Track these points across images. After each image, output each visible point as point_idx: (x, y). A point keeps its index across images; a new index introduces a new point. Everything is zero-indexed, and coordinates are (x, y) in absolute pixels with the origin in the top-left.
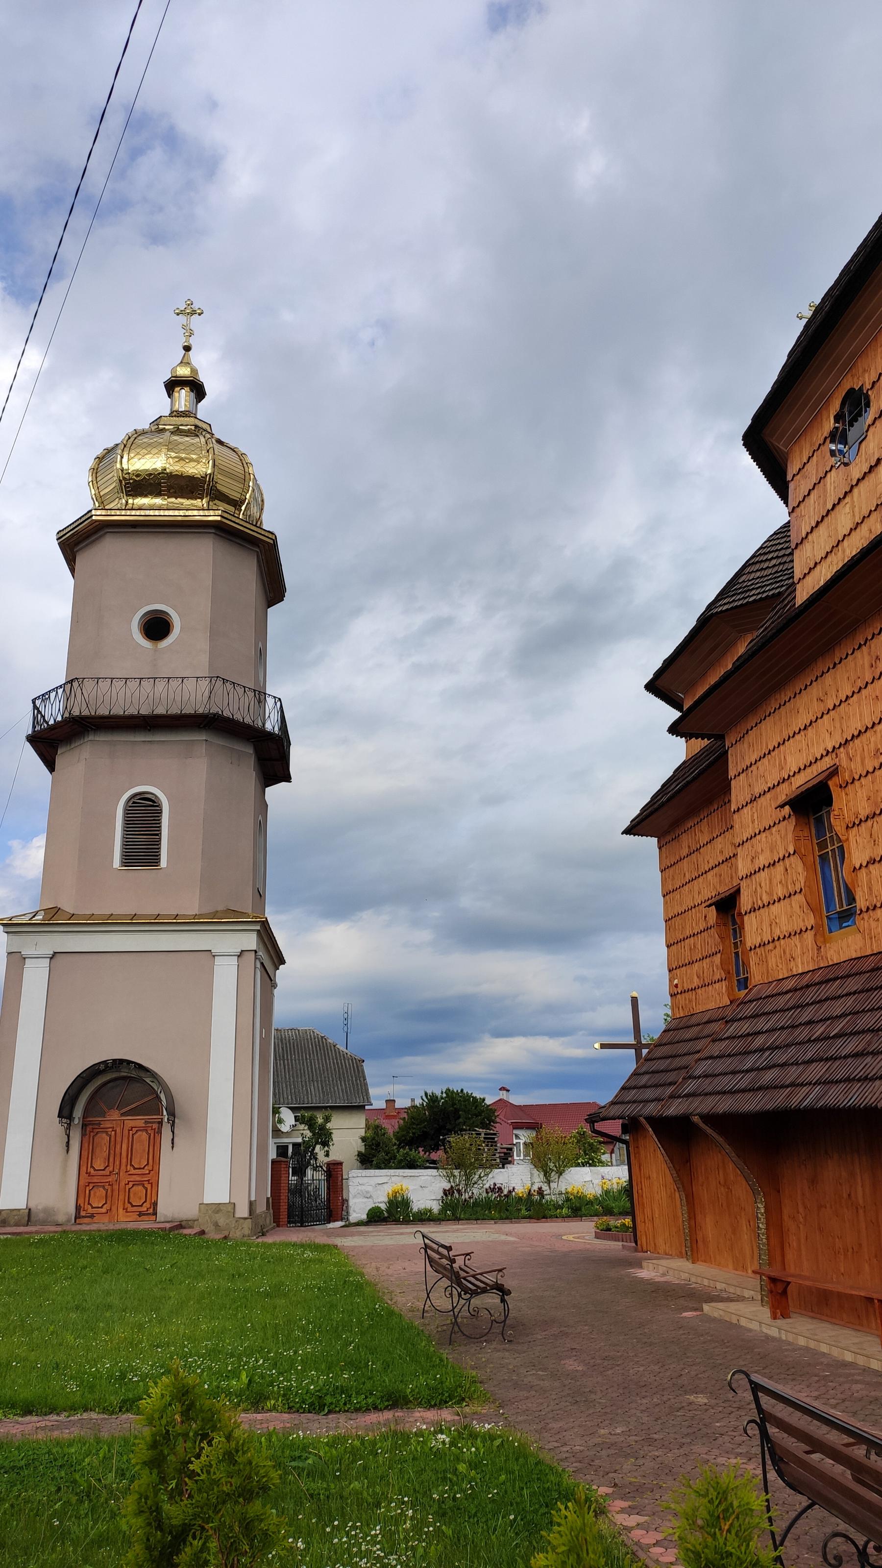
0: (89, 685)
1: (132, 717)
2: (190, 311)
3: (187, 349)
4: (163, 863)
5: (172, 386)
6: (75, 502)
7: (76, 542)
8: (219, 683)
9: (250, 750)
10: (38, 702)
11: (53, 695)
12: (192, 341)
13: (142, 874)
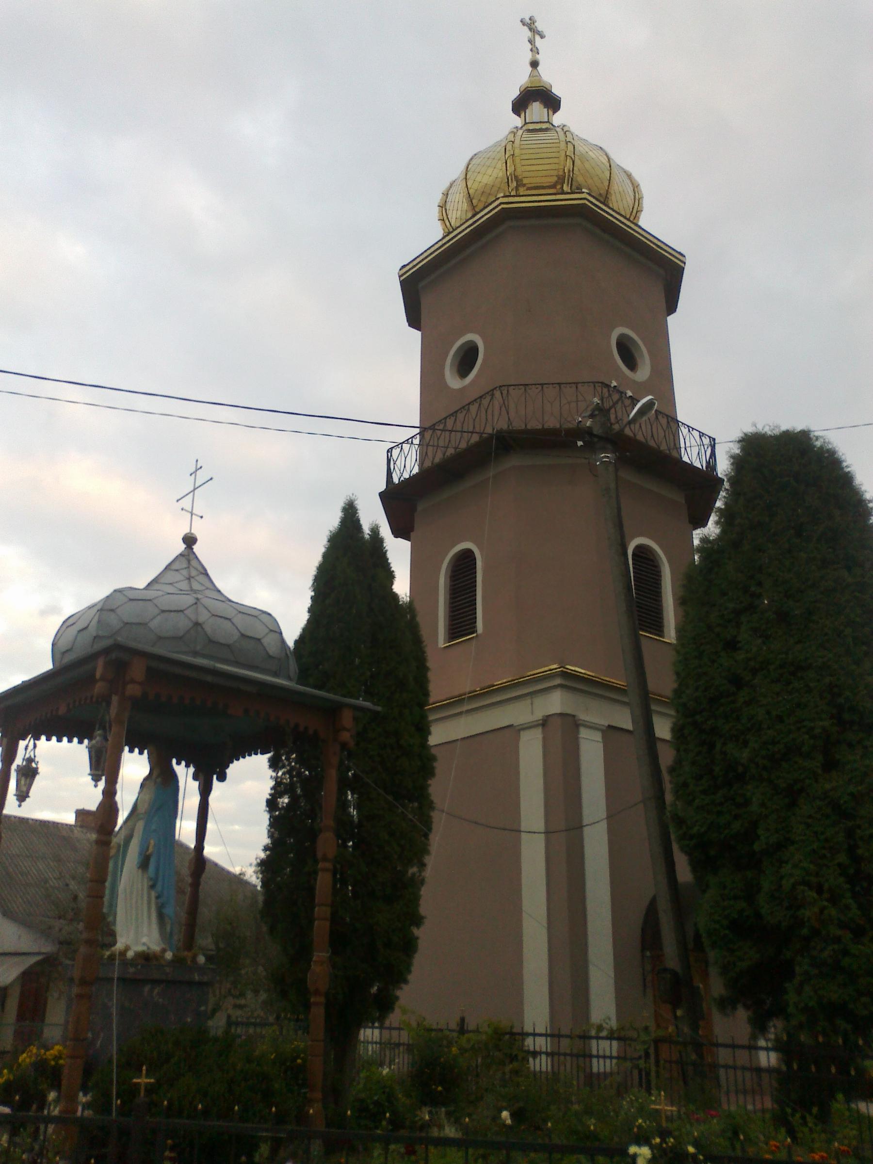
3: (534, 64)
10: (396, 452)
12: (539, 57)
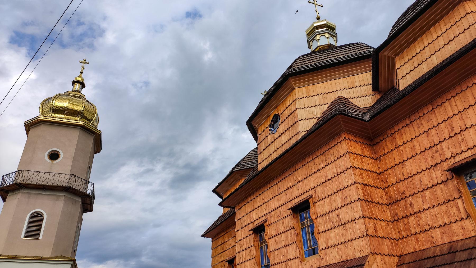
0: (25, 173)
1: (39, 185)
2: (85, 62)
3: (82, 73)
4: (41, 238)
5: (74, 82)
6: (34, 112)
7: (30, 126)
8: (73, 176)
9: (80, 200)
10: (4, 177)
11: (14, 174)
12: (84, 71)
13: (32, 242)
